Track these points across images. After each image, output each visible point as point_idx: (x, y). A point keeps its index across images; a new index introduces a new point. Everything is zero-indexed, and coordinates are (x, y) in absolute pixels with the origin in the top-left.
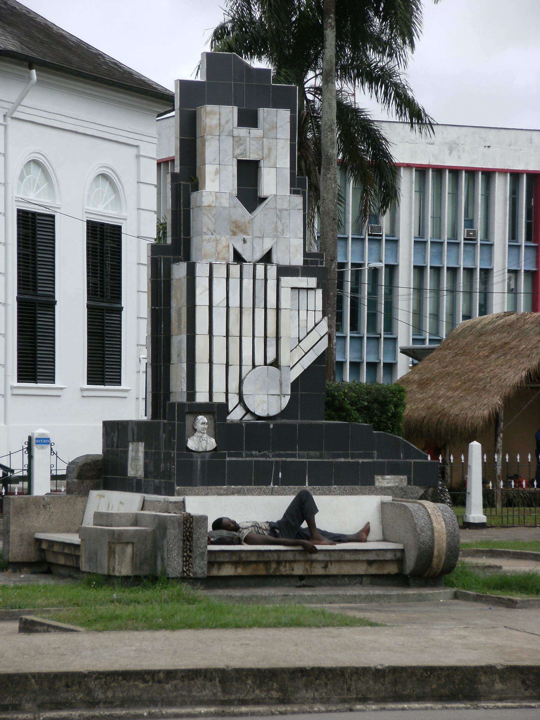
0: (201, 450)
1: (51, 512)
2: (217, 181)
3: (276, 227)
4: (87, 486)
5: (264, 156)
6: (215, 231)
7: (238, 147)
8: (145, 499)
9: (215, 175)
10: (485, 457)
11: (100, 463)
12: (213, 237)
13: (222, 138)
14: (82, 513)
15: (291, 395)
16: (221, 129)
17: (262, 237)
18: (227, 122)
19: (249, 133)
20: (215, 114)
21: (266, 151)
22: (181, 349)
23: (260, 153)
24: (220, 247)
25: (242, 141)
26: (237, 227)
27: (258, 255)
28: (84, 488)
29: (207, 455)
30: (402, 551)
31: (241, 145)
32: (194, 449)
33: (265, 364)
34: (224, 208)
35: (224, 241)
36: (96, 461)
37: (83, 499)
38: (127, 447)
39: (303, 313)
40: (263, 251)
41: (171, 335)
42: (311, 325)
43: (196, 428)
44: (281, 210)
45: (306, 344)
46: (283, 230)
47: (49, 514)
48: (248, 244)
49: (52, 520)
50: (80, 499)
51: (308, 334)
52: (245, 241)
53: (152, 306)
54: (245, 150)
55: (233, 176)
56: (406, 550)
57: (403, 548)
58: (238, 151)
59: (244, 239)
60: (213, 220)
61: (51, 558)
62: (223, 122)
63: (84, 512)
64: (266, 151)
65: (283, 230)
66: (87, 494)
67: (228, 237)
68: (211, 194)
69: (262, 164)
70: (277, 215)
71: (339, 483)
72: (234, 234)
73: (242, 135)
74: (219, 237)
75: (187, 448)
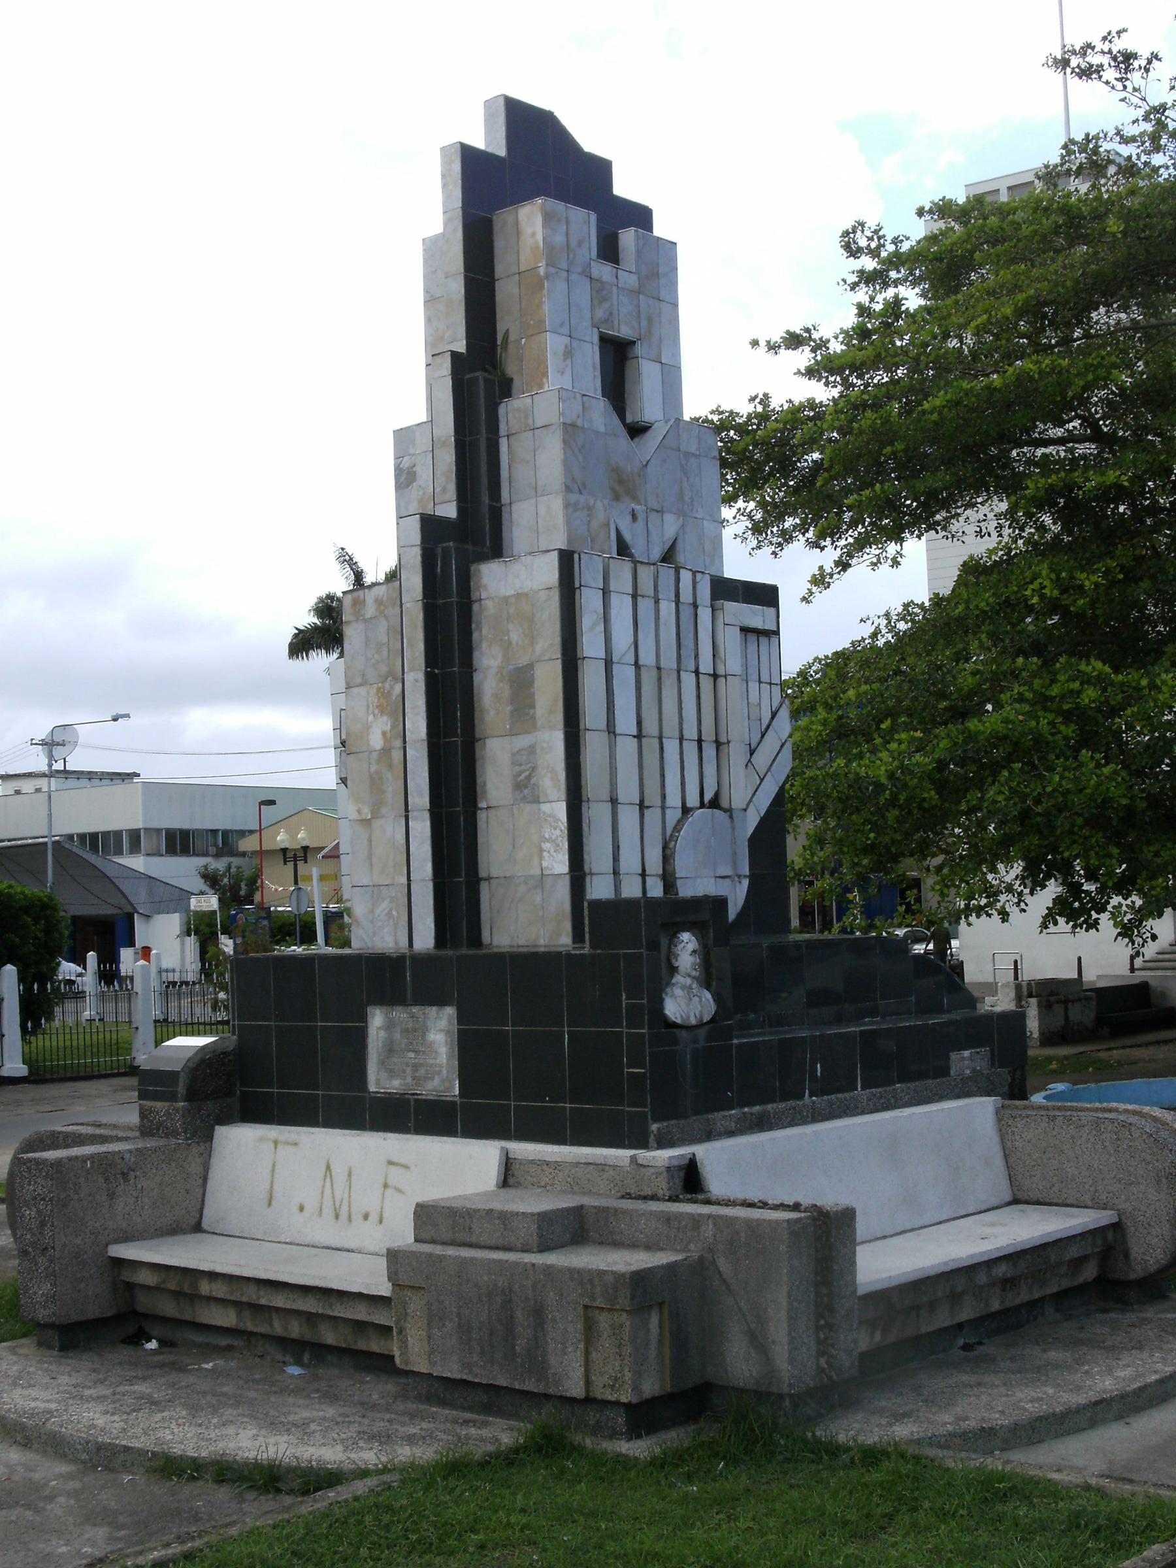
0: (693, 1021)
1: (139, 1186)
2: (568, 372)
3: (681, 490)
4: (209, 1115)
5: (642, 333)
6: (584, 486)
7: (601, 302)
8: (511, 1155)
9: (565, 360)
10: (21, 988)
11: (231, 1058)
12: (582, 499)
13: (573, 277)
14: (200, 1181)
15: (753, 878)
16: (571, 256)
17: (660, 512)
18: (580, 244)
19: (617, 277)
20: (559, 220)
21: (644, 323)
22: (534, 769)
23: (635, 324)
24: (595, 524)
25: (605, 292)
26: (620, 481)
27: (657, 553)
28: (202, 1121)
29: (702, 1032)
30: (1117, 1227)
31: (604, 300)
32: (679, 1021)
33: (702, 806)
34: (597, 433)
35: (600, 515)
36: (222, 1053)
37: (202, 1148)
38: (363, 1018)
39: (754, 686)
40: (664, 543)
41: (477, 735)
42: (766, 716)
43: (676, 965)
44: (688, 455)
45: (761, 759)
46: (692, 499)
47: (135, 1194)
48: (640, 523)
49: (143, 1208)
50: (195, 1150)
51: (763, 736)
52: (634, 517)
53: (427, 667)
54: (611, 313)
55: (594, 368)
56: (1128, 1223)
57: (1115, 1220)
58: (600, 314)
59: (633, 510)
60: (581, 459)
61: (144, 1303)
62: (574, 243)
63: (205, 1179)
64: (644, 323)
65: (692, 499)
66: (209, 1138)
67: (606, 502)
68: (575, 398)
69: (639, 350)
70: (682, 466)
71: (907, 1077)
72: (617, 498)
73: (605, 279)
74: (592, 502)
75: (665, 1018)
